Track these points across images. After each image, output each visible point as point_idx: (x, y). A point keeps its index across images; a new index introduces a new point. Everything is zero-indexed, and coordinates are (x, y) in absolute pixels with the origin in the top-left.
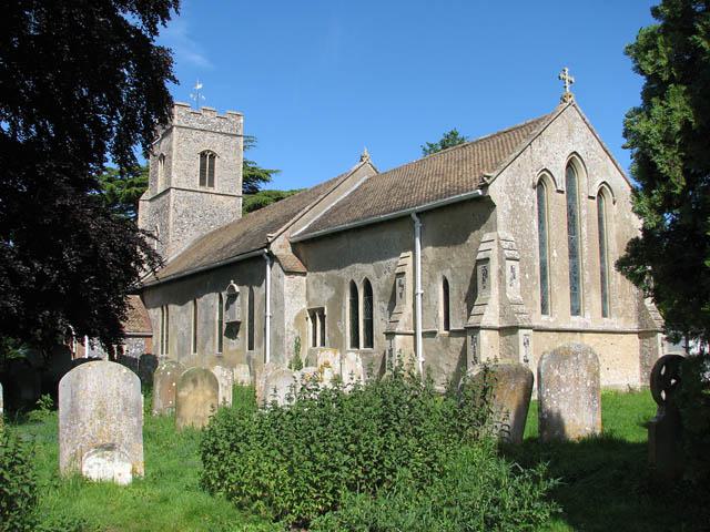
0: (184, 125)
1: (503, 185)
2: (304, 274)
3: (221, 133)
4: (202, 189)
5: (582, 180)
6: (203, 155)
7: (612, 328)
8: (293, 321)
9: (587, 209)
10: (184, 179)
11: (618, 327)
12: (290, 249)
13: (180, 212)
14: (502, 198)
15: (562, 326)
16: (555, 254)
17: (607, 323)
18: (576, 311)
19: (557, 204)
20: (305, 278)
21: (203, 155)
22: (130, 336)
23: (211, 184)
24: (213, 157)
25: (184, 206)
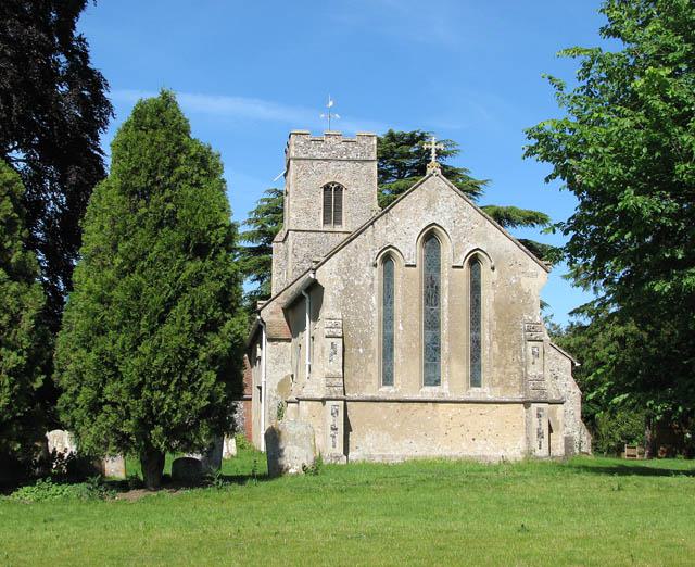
0: (304, 156)
1: (334, 268)
2: (289, 340)
3: (349, 160)
4: (327, 228)
5: (446, 251)
6: (327, 188)
7: (482, 398)
8: (276, 387)
9: (454, 283)
10: (304, 218)
11: (490, 397)
12: (282, 314)
13: (300, 258)
14: (331, 280)
15: (407, 396)
16: (401, 328)
17: (475, 394)
18: (388, 379)
19: (408, 284)
20: (290, 344)
21: (327, 188)
22: (520, 403)
23: (338, 221)
24: (339, 189)
25: (305, 250)
